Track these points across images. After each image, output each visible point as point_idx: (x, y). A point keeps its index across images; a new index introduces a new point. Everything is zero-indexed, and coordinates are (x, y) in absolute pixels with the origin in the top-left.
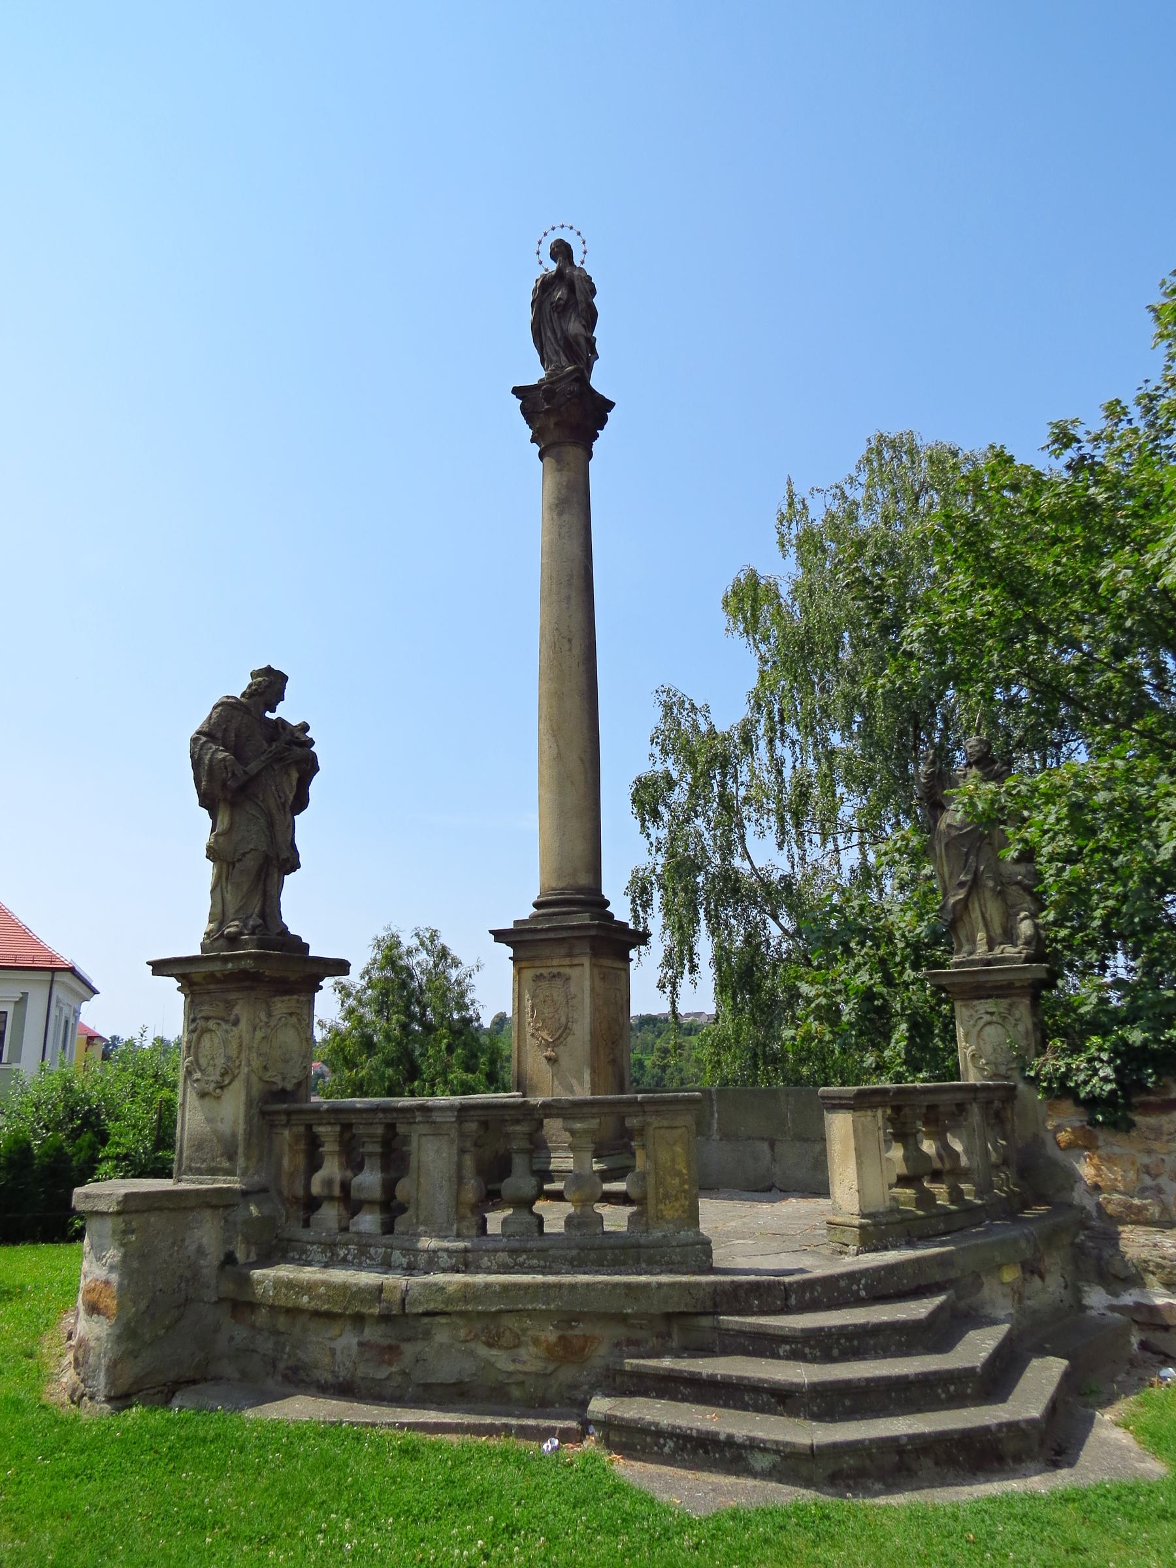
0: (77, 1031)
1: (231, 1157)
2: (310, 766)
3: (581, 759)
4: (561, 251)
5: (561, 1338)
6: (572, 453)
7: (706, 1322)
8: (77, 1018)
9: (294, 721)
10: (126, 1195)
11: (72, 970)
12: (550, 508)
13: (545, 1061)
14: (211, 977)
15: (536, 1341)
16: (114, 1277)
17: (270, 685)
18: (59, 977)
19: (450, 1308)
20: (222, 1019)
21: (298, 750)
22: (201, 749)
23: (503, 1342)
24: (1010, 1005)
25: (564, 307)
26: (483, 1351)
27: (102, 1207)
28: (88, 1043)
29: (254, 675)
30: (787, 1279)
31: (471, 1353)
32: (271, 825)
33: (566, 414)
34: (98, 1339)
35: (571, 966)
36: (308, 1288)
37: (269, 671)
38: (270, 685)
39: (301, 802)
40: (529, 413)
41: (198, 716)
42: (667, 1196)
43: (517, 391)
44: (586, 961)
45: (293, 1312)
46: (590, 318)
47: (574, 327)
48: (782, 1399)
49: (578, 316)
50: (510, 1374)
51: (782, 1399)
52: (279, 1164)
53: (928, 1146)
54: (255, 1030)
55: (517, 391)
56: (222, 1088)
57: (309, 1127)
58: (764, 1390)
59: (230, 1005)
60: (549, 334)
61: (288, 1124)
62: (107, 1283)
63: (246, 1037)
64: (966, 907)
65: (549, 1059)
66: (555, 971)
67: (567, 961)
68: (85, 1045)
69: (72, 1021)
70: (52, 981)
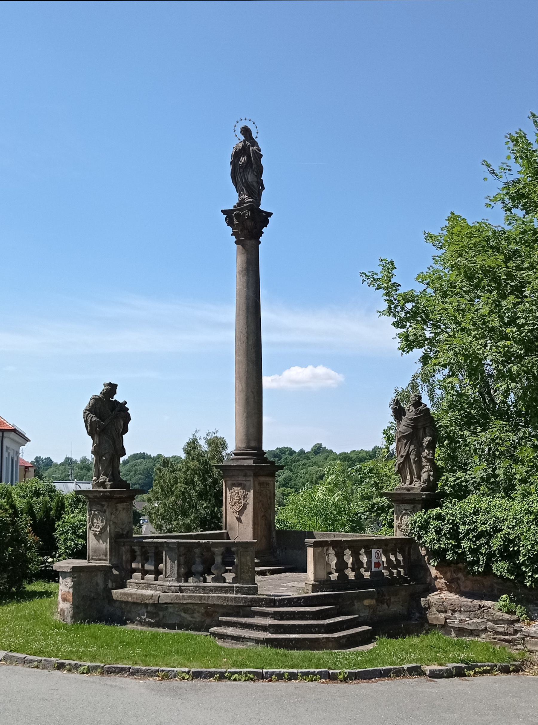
0: (19, 464)
1: (106, 556)
2: (128, 418)
3: (252, 392)
4: (246, 131)
5: (206, 611)
6: (249, 243)
7: (248, 608)
8: (18, 457)
9: (121, 401)
10: (73, 567)
11: (15, 431)
12: (239, 272)
13: (235, 518)
14: (95, 497)
15: (198, 612)
16: (71, 590)
17: (112, 389)
18: (6, 434)
19: (172, 602)
20: (100, 511)
21: (122, 413)
22: (87, 416)
23: (189, 612)
24: (414, 507)
25: (247, 166)
26: (183, 614)
27: (65, 570)
28: (25, 471)
29: (105, 385)
30: (276, 598)
31: (180, 615)
32: (114, 443)
33: (248, 223)
34: (67, 608)
35: (246, 481)
36: (131, 595)
37: (110, 384)
38: (112, 389)
39: (125, 430)
40: (230, 222)
41: (85, 403)
42: (244, 572)
43: (224, 212)
44: (251, 479)
45: (127, 603)
46: (260, 170)
47: (251, 178)
48: (264, 628)
49: (253, 171)
50: (191, 621)
51: (264, 628)
52: (122, 559)
53: (393, 558)
54: (111, 514)
55: (224, 212)
56: (101, 533)
57: (131, 547)
58: (259, 626)
59: (103, 506)
60: (239, 180)
61: (124, 545)
62: (69, 592)
63: (109, 517)
64: (403, 465)
65: (237, 518)
66: (240, 482)
67: (244, 479)
68: (23, 472)
69: (15, 459)
70: (3, 437)
